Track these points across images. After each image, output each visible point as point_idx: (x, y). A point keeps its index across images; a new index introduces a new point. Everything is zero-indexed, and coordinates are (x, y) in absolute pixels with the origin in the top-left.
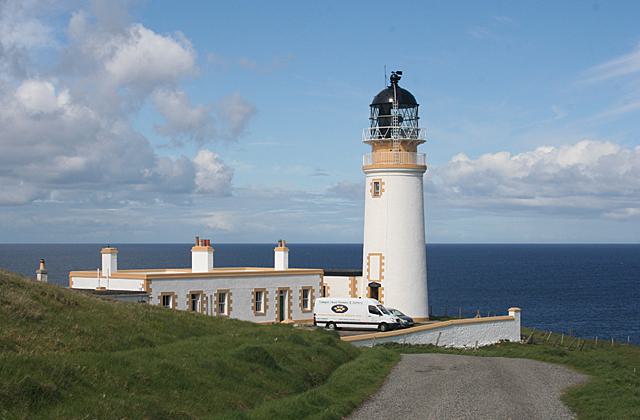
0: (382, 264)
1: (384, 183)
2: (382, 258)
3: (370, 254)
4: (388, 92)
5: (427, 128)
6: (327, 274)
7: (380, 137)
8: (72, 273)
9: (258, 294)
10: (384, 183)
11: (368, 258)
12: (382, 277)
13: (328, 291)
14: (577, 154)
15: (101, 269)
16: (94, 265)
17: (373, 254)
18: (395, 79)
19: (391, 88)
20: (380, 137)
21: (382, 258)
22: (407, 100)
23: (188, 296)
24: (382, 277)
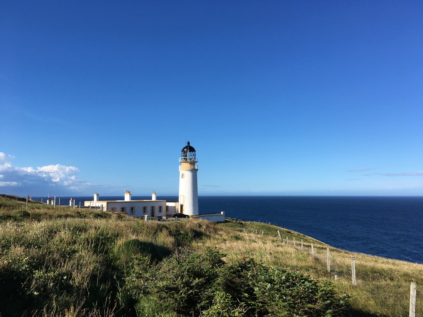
0: (184, 199)
1: (185, 174)
2: (184, 197)
3: (181, 196)
4: (186, 147)
5: (197, 153)
6: (167, 202)
7: (184, 161)
8: (85, 202)
9: (145, 208)
10: (185, 174)
11: (180, 197)
12: (184, 203)
13: (143, 209)
14: (108, 309)
15: (93, 201)
16: (91, 199)
17: (181, 196)
18: (189, 143)
19: (187, 146)
20: (184, 161)
21: (184, 197)
22: (192, 149)
23: (150, 207)
24: (184, 203)
